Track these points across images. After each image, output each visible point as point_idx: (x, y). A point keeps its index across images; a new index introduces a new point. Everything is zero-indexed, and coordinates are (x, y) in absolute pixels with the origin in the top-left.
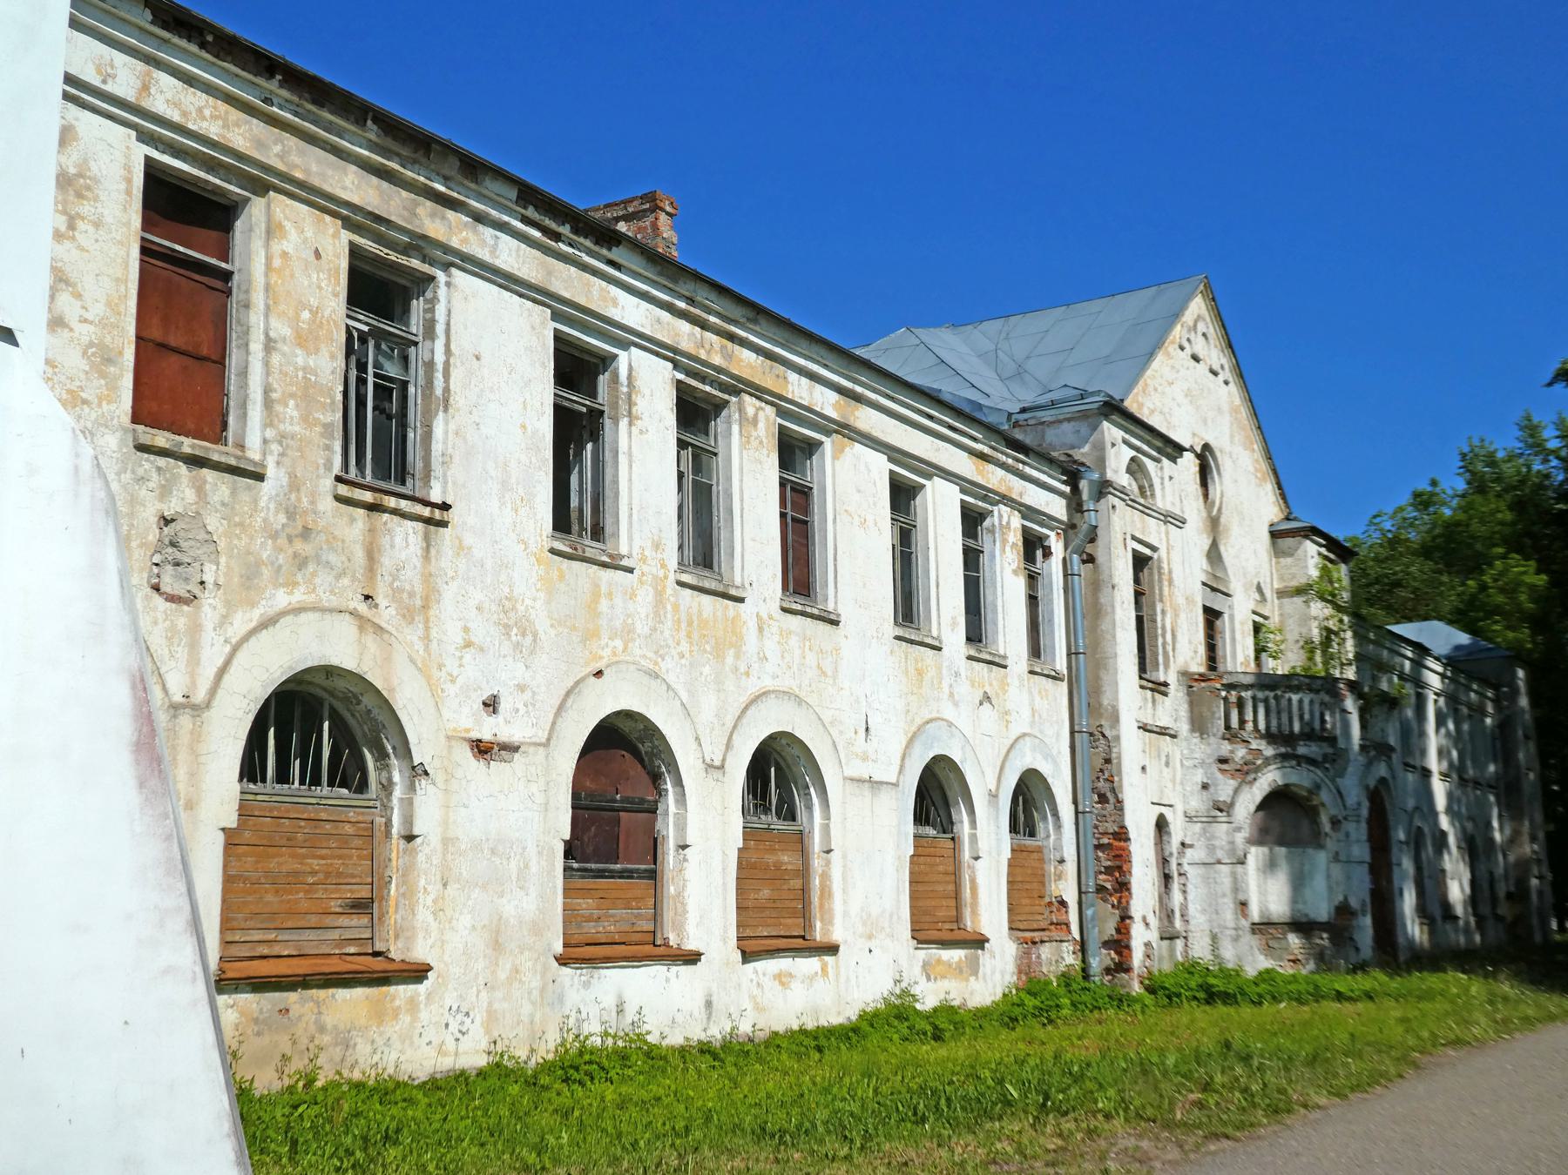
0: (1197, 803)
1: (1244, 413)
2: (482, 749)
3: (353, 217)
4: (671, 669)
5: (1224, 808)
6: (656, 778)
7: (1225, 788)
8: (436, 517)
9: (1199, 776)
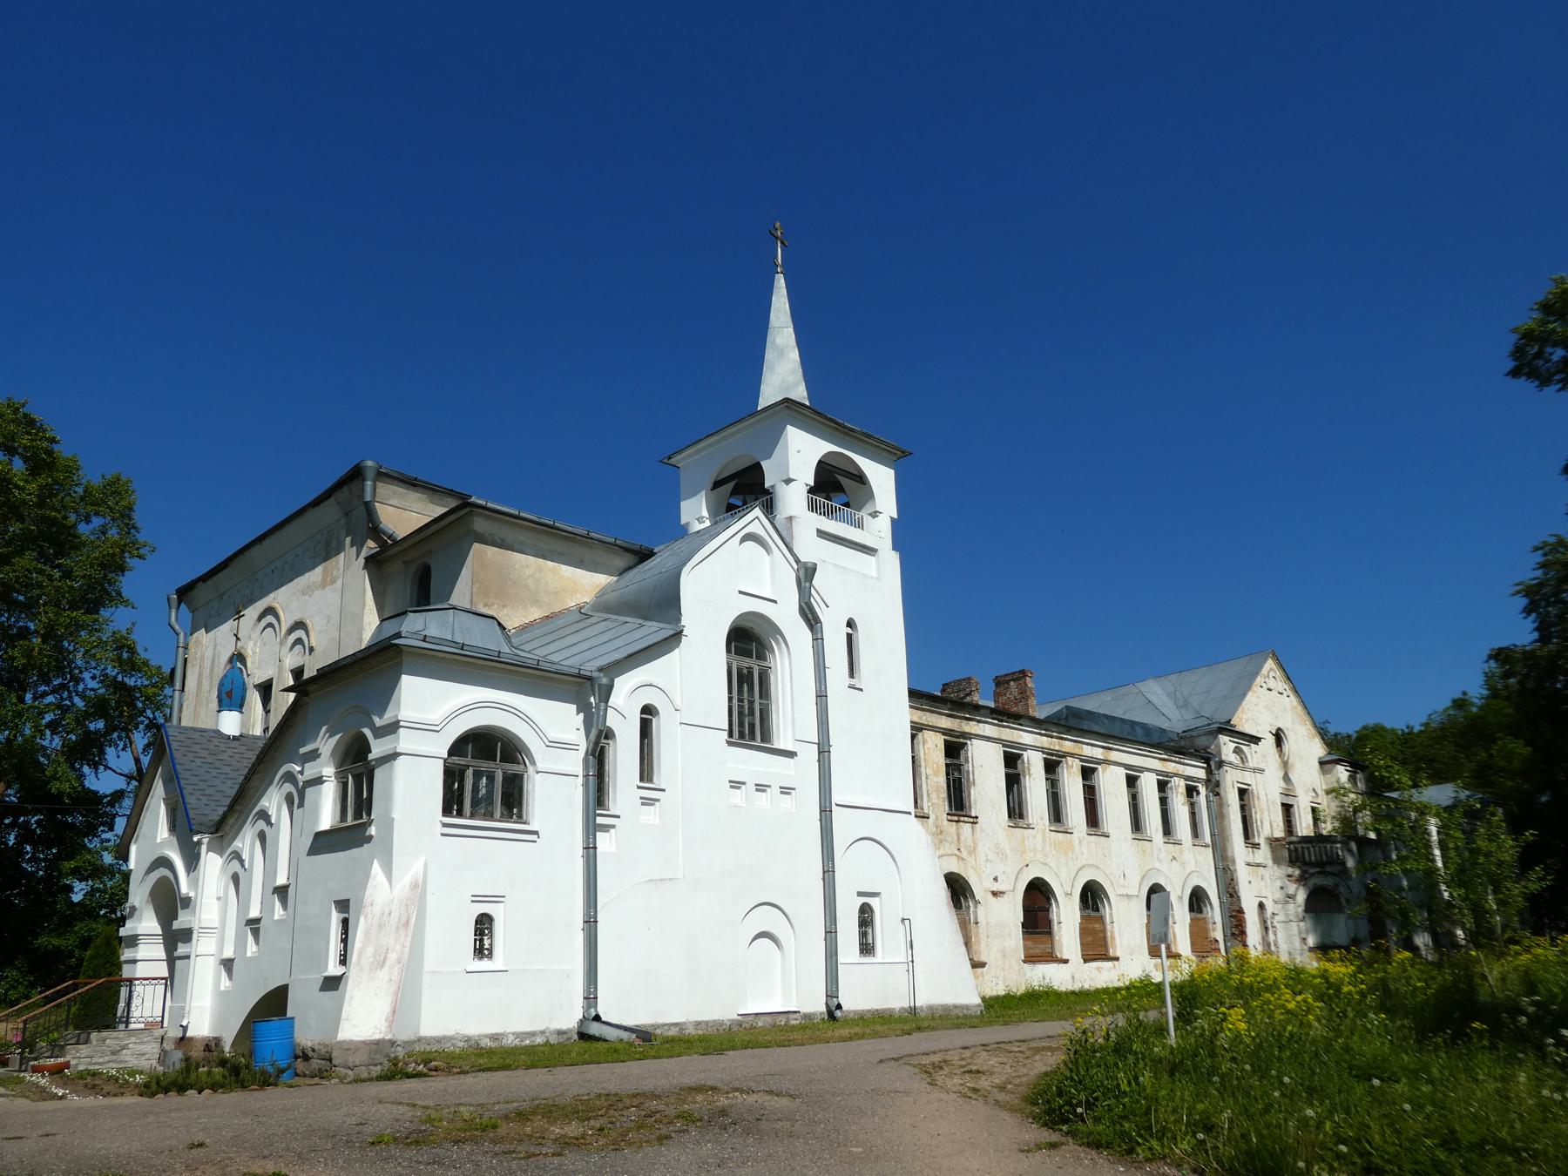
0: (1279, 895)
1: (1300, 708)
2: (995, 894)
3: (945, 732)
4: (1051, 861)
5: (1291, 897)
6: (1048, 900)
7: (1292, 888)
8: (974, 821)
9: (1279, 884)
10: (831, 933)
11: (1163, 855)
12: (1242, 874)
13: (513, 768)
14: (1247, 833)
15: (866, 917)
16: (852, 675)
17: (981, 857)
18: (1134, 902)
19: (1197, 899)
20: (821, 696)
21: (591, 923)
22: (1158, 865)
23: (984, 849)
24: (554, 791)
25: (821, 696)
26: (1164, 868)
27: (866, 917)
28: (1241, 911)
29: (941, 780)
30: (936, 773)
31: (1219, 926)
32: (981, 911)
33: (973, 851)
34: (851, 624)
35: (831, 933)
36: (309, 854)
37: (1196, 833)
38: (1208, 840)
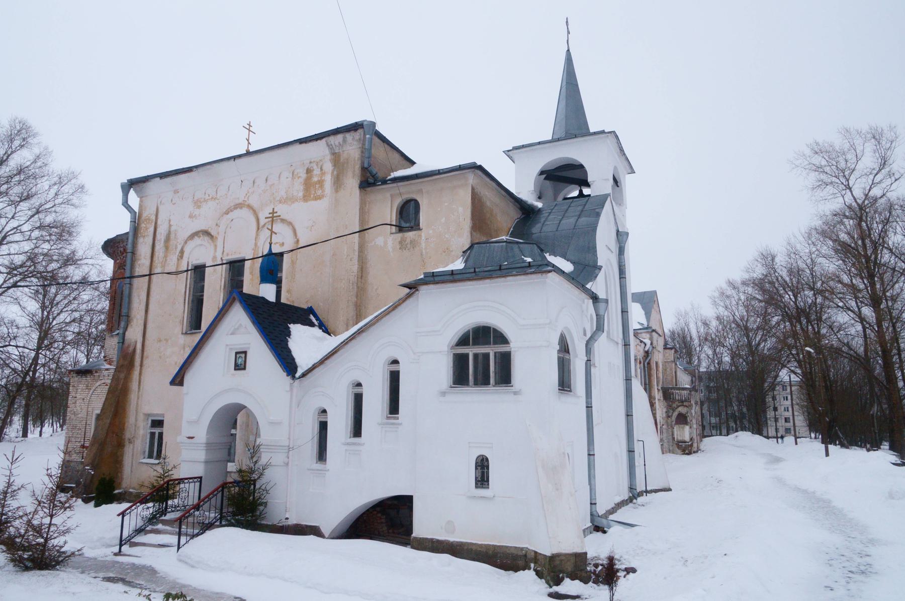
13: (502, 348)
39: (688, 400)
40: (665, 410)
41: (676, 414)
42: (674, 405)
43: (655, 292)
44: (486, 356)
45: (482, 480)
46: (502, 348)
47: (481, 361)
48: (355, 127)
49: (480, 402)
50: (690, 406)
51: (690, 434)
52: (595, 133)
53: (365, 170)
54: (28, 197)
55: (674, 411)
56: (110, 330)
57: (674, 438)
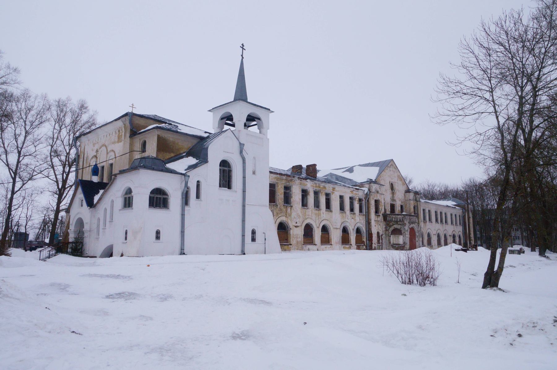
10: (243, 236)
11: (349, 217)
12: (373, 223)
13: (165, 197)
14: (377, 212)
15: (253, 232)
16: (96, 257)
17: (293, 216)
18: (338, 230)
19: (358, 231)
20: (244, 177)
21: (183, 232)
22: (347, 220)
23: (294, 215)
24: (175, 200)
25: (244, 177)
26: (349, 221)
27: (253, 232)
28: (371, 234)
29: (282, 196)
30: (281, 194)
31: (365, 237)
32: (291, 231)
33: (290, 215)
34: (254, 158)
35: (243, 236)
36: (484, 287)
37: (361, 211)
38: (364, 213)
39: (403, 221)
40: (384, 227)
41: (392, 228)
42: (391, 224)
43: (315, 165)
44: (160, 198)
45: (158, 238)
46: (165, 197)
47: (158, 199)
48: (126, 115)
49: (158, 213)
50: (404, 225)
51: (403, 240)
52: (250, 103)
53: (131, 130)
54: (30, 110)
55: (390, 227)
56: (116, 175)
57: (390, 243)
